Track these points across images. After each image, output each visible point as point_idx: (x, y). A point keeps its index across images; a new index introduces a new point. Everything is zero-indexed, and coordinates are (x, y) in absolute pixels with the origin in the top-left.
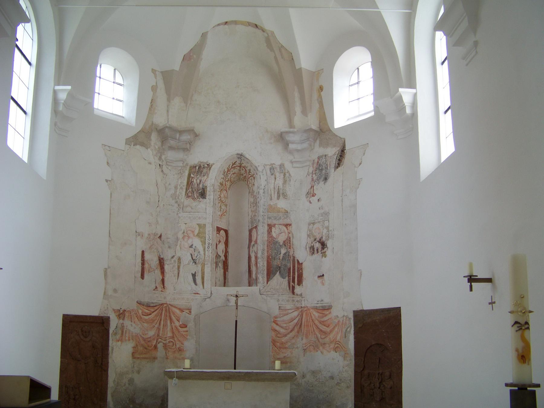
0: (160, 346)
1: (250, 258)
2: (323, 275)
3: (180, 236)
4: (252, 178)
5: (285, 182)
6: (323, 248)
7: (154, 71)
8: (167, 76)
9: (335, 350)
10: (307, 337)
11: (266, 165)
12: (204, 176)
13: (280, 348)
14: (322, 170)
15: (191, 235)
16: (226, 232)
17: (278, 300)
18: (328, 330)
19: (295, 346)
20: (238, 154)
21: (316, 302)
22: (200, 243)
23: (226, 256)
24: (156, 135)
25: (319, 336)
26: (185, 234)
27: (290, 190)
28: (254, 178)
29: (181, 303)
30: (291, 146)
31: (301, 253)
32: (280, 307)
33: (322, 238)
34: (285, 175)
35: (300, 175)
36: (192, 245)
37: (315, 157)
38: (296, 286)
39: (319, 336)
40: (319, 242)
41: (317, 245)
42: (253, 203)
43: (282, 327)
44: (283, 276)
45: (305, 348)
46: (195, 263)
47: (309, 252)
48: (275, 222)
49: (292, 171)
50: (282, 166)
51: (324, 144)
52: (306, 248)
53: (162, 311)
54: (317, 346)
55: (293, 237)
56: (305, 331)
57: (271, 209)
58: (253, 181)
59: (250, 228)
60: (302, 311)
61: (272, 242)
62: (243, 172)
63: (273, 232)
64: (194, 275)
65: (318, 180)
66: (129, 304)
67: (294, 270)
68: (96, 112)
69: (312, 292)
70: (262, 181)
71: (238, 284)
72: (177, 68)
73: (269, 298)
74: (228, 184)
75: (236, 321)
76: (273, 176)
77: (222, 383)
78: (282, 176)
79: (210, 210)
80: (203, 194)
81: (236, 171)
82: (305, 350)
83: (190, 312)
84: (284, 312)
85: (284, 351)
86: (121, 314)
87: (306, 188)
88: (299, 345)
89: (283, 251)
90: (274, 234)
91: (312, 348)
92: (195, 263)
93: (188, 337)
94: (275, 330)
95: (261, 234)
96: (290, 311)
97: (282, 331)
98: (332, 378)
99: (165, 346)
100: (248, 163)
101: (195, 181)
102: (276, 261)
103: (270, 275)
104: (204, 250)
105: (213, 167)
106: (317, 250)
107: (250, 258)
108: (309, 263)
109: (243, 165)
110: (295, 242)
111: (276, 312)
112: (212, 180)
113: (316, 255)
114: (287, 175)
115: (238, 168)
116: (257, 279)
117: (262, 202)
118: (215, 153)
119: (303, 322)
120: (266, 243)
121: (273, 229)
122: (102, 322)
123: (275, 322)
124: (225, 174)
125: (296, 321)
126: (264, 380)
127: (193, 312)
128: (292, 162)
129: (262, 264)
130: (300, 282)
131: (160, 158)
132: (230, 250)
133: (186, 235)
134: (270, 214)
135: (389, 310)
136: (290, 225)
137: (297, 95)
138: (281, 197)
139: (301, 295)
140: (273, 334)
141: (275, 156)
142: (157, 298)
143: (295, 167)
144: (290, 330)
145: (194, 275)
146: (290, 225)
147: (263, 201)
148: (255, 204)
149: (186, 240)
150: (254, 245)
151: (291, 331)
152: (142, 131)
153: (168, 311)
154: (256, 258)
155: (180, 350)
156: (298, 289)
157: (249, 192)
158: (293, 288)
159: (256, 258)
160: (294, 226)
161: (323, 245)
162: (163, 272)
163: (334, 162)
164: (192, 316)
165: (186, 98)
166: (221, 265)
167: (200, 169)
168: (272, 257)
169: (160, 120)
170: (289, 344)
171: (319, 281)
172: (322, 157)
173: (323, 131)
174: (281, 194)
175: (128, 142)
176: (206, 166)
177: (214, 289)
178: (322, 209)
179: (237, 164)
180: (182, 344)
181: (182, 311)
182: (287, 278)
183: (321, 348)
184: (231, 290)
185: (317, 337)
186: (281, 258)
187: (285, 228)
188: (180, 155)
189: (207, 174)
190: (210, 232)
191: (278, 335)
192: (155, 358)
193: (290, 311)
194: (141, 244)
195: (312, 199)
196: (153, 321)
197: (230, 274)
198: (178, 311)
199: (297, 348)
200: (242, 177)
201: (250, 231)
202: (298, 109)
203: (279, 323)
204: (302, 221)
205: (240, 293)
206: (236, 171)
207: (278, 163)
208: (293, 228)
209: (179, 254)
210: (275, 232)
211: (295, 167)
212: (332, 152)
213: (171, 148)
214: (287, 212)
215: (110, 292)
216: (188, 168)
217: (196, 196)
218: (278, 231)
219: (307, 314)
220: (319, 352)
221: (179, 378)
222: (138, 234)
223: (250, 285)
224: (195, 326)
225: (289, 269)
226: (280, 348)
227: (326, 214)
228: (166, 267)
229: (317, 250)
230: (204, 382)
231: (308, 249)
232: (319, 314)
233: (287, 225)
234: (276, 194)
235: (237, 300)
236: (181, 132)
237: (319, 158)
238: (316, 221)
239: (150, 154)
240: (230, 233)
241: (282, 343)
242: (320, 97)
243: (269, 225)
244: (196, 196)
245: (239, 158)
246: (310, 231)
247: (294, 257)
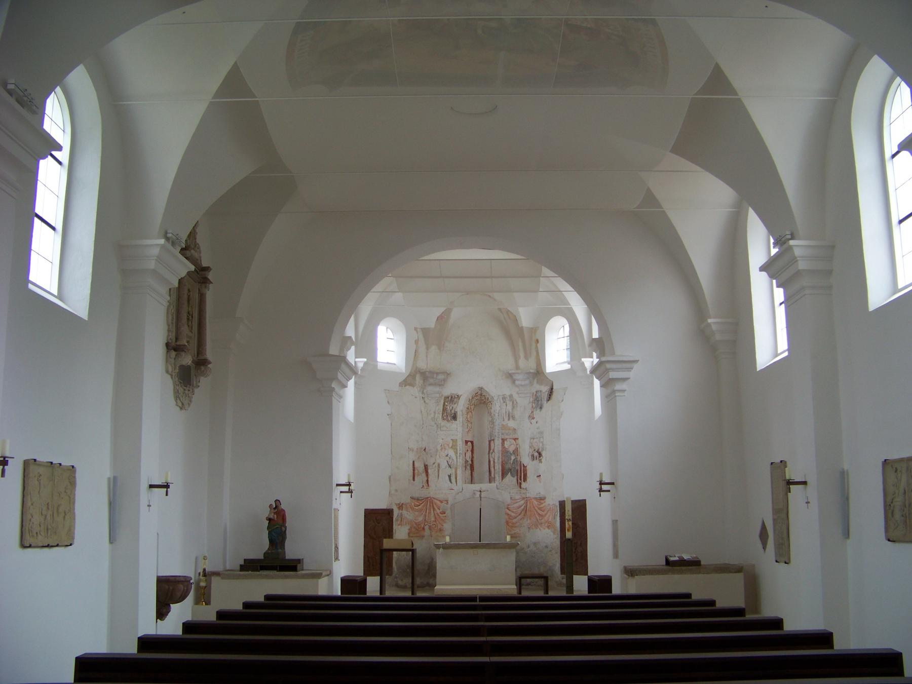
0: (427, 528)
3: (439, 448)
5: (513, 407)
7: (416, 329)
8: (425, 332)
9: (548, 527)
16: (472, 442)
18: (544, 513)
24: (420, 377)
27: (517, 413)
29: (441, 496)
30: (517, 382)
31: (526, 460)
35: (524, 403)
37: (534, 391)
41: (536, 454)
48: (507, 437)
49: (518, 400)
50: (511, 396)
51: (540, 382)
53: (426, 503)
54: (537, 525)
57: (504, 427)
60: (527, 500)
61: (505, 452)
64: (450, 476)
66: (405, 499)
68: (380, 366)
69: (533, 487)
71: (481, 482)
72: (432, 325)
73: (503, 491)
77: (471, 551)
79: (460, 429)
80: (455, 418)
86: (400, 507)
89: (513, 458)
90: (506, 446)
95: (497, 445)
98: (546, 547)
99: (430, 528)
103: (504, 475)
108: (531, 467)
111: (509, 501)
112: (460, 407)
117: (497, 423)
118: (463, 386)
122: (388, 513)
126: (498, 548)
129: (498, 467)
130: (525, 480)
131: (423, 393)
133: (443, 448)
135: (579, 501)
137: (520, 344)
141: (506, 389)
142: (424, 493)
145: (450, 476)
147: (498, 422)
148: (492, 423)
152: (410, 375)
153: (432, 502)
155: (441, 530)
156: (524, 485)
161: (540, 454)
162: (427, 475)
163: (546, 396)
164: (449, 506)
165: (441, 347)
166: (469, 467)
167: (452, 399)
169: (422, 365)
171: (537, 479)
173: (539, 373)
174: (511, 417)
175: (401, 384)
177: (465, 486)
181: (441, 502)
184: (476, 487)
188: (437, 389)
189: (457, 403)
190: (460, 444)
192: (423, 536)
194: (412, 456)
196: (420, 510)
197: (475, 474)
198: (438, 502)
201: (490, 442)
202: (522, 354)
204: (526, 434)
205: (483, 489)
207: (508, 393)
209: (438, 461)
210: (507, 444)
212: (545, 389)
213: (430, 385)
215: (393, 492)
222: (410, 449)
223: (490, 482)
227: (541, 433)
228: (429, 471)
233: (515, 439)
236: (437, 374)
239: (415, 391)
242: (537, 347)
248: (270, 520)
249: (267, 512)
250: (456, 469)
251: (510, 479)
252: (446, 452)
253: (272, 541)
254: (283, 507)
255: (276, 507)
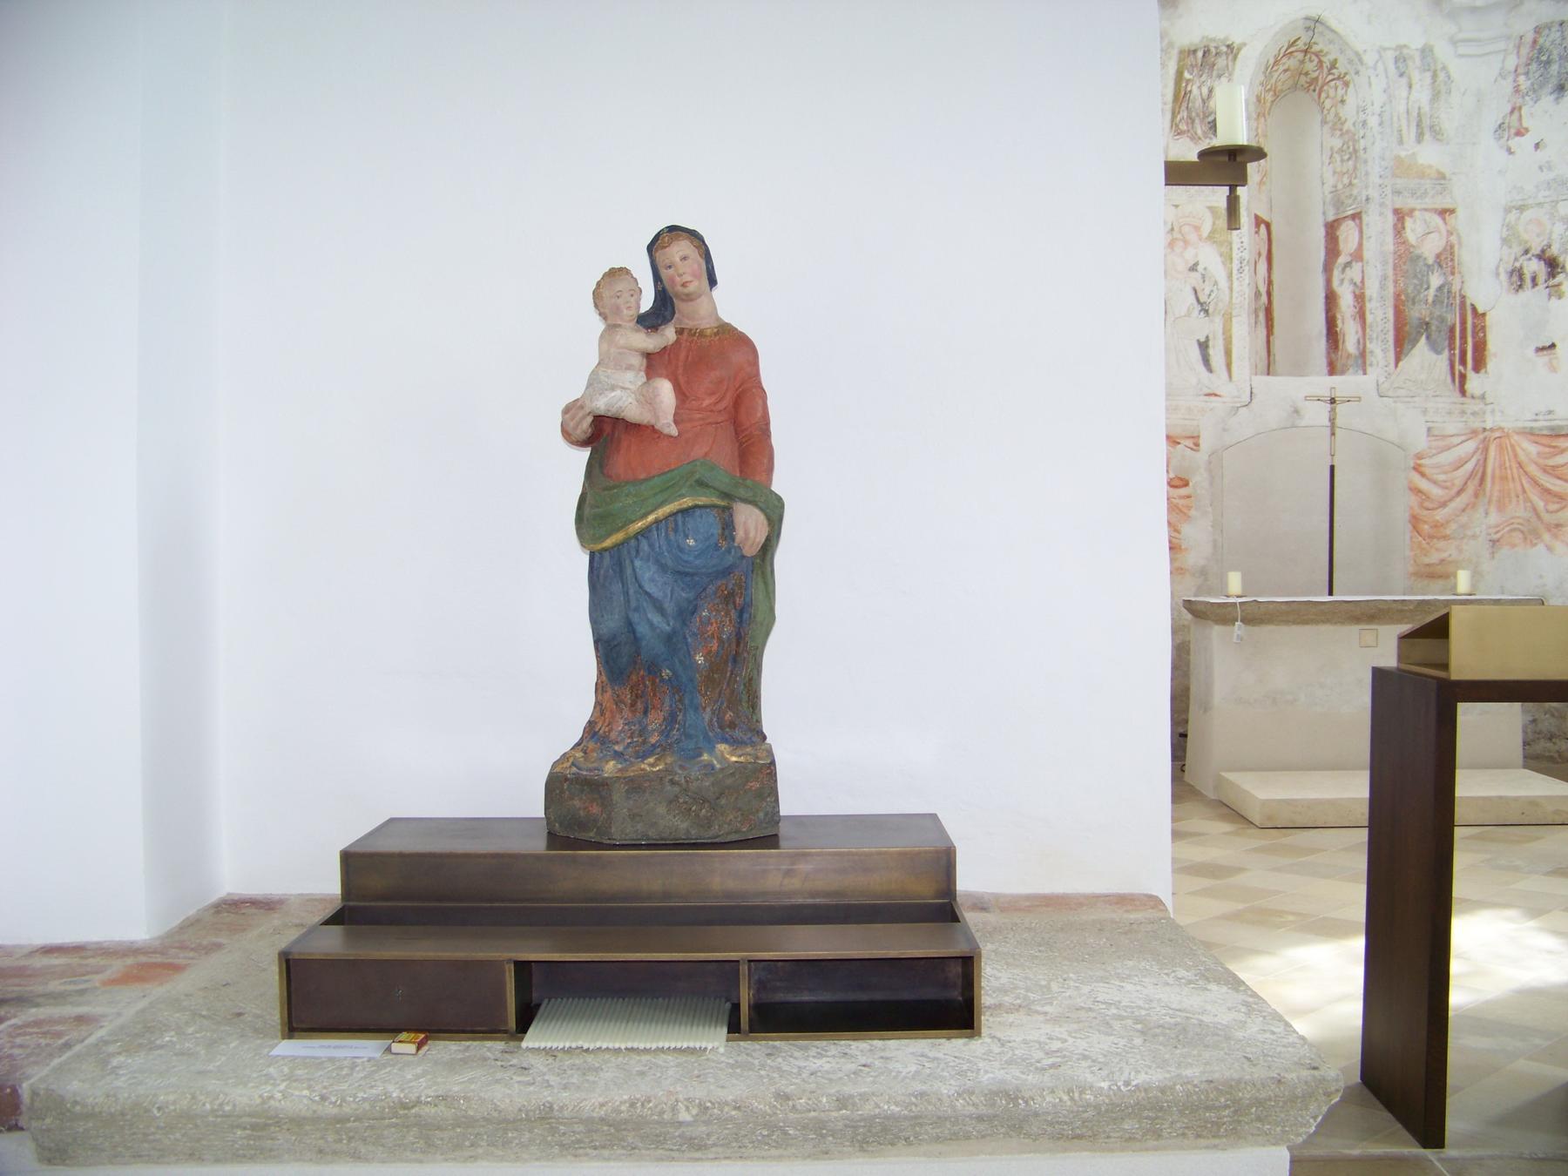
1: (1331, 299)
2: (1553, 346)
4: (1339, 83)
5: (1435, 96)
6: (1552, 275)
10: (1501, 508)
11: (1385, 49)
12: (1219, 76)
13: (1431, 537)
14: (1548, 62)
15: (1193, 237)
17: (1425, 412)
19: (1469, 533)
20: (1307, 18)
21: (1530, 416)
22: (1219, 259)
23: (1269, 294)
25: (1540, 505)
26: (1176, 235)
27: (1450, 117)
28: (1346, 84)
31: (1484, 287)
32: (1429, 429)
33: (1549, 246)
34: (1434, 76)
36: (1196, 264)
38: (1470, 374)
39: (1540, 505)
40: (1540, 257)
41: (1534, 266)
42: (1341, 150)
43: (1435, 482)
44: (1435, 348)
45: (1495, 537)
46: (1206, 311)
47: (1505, 284)
49: (1456, 67)
50: (1426, 51)
52: (1498, 275)
55: (1460, 244)
56: (1496, 494)
57: (1401, 167)
58: (1340, 92)
59: (1331, 218)
60: (1486, 439)
61: (1405, 258)
62: (1310, 66)
63: (1408, 230)
64: (1204, 346)
65: (1535, 91)
67: (1463, 330)
70: (1371, 97)
71: (1298, 369)
74: (1269, 97)
75: (1332, 468)
76: (1404, 81)
77: (1354, 629)
78: (1428, 80)
81: (1291, 63)
82: (1494, 542)
83: (1197, 445)
84: (1441, 443)
85: (1441, 544)
87: (1497, 110)
88: (1477, 530)
89: (1436, 280)
91: (1517, 537)
92: (1206, 311)
93: (1193, 513)
94: (1417, 491)
95: (1375, 239)
96: (1456, 440)
97: (1436, 492)
100: (1331, 42)
101: (1195, 91)
102: (1417, 307)
103: (1402, 343)
104: (1230, 276)
105: (1242, 52)
106: (1534, 279)
107: (1331, 299)
108: (1508, 317)
109: (1315, 48)
110: (1464, 256)
111: (1420, 442)
113: (1528, 294)
114: (1441, 76)
115: (1300, 56)
116: (1363, 354)
119: (1489, 471)
120: (1391, 261)
121: (1408, 222)
123: (1417, 468)
124: (1269, 69)
125: (1469, 466)
127: (1205, 444)
128: (1454, 42)
129: (1381, 315)
130: (1479, 365)
132: (1275, 277)
134: (1399, 181)
136: (1452, 211)
138: (1427, 136)
139: (1483, 397)
140: (1413, 500)
143: (1462, 56)
144: (1455, 490)
146: (1452, 211)
147: (1377, 148)
148: (1352, 152)
149: (1178, 249)
150: (1348, 265)
151: (1459, 493)
154: (1360, 298)
156: (1474, 383)
157: (1324, 122)
158: (1463, 377)
159: (1360, 298)
160: (1460, 212)
168: (1407, 295)
170: (1454, 526)
171: (1543, 359)
172: (1549, 26)
176: (1224, 49)
178: (1550, 169)
179: (1300, 45)
180: (1178, 532)
182: (1446, 353)
183: (1546, 536)
185: (1535, 510)
186: (1430, 299)
187: (1437, 220)
189: (1227, 73)
191: (1427, 504)
193: (1456, 440)
195: (1515, 142)
199: (1474, 537)
200: (1303, 79)
201: (1332, 229)
203: (1427, 471)
205: (1338, 394)
206: (1291, 63)
207: (1415, 42)
208: (1460, 220)
210: (1413, 230)
211: (1462, 56)
214: (1444, 178)
216: (1175, 53)
217: (1199, 132)
218: (1420, 229)
219: (1501, 448)
220: (1541, 547)
221: (1247, 621)
224: (1211, 484)
225: (1452, 330)
226: (1431, 537)
229: (1534, 279)
230: (1326, 629)
231: (1504, 277)
232: (1541, 448)
233: (1444, 213)
234: (1413, 129)
235: (1333, 410)
237: (1538, 30)
238: (1530, 202)
240: (1274, 228)
241: (1436, 526)
243: (1396, 212)
244: (1199, 132)
245: (1308, 29)
246: (1509, 227)
247: (1463, 297)
248: (602, 435)
249: (570, 357)
250: (1228, 319)
251: (1426, 361)
252: (1189, 255)
253: (622, 660)
254: (731, 304)
255: (665, 306)
